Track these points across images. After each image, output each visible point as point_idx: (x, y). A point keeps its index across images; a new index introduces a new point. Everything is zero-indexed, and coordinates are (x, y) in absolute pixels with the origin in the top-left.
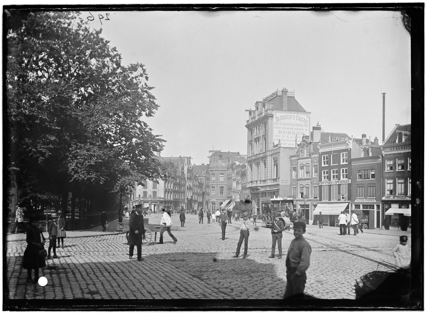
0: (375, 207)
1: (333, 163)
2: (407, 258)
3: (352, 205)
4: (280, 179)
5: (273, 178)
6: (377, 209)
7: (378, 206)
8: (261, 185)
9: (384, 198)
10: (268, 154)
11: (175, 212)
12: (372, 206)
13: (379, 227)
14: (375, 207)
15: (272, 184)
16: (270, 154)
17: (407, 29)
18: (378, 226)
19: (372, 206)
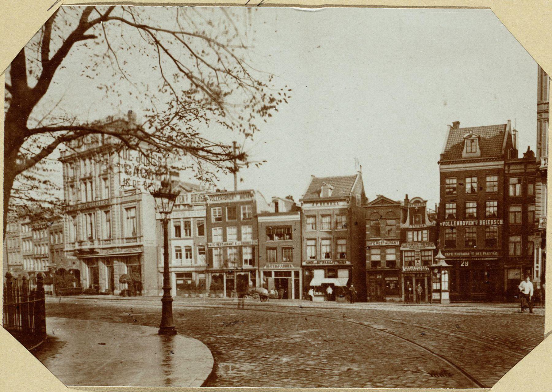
0: (293, 274)
1: (229, 218)
2: (31, 120)
3: (259, 272)
4: (144, 238)
5: (126, 236)
6: (295, 277)
7: (297, 274)
8: (101, 247)
9: (304, 264)
10: (115, 201)
11: (140, 241)
12: (289, 274)
13: (299, 298)
14: (293, 274)
15: (125, 245)
16: (119, 202)
17: (79, 383)
18: (297, 297)
19: (289, 274)
